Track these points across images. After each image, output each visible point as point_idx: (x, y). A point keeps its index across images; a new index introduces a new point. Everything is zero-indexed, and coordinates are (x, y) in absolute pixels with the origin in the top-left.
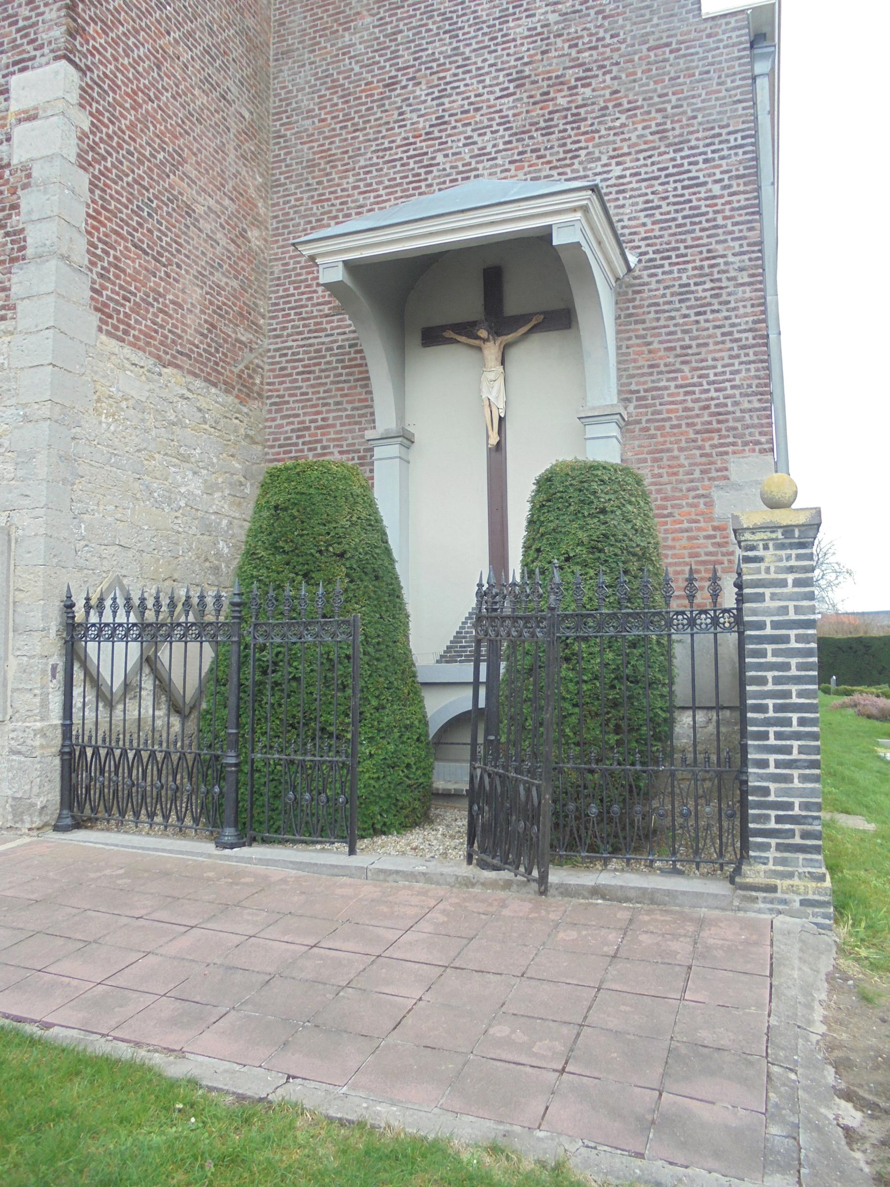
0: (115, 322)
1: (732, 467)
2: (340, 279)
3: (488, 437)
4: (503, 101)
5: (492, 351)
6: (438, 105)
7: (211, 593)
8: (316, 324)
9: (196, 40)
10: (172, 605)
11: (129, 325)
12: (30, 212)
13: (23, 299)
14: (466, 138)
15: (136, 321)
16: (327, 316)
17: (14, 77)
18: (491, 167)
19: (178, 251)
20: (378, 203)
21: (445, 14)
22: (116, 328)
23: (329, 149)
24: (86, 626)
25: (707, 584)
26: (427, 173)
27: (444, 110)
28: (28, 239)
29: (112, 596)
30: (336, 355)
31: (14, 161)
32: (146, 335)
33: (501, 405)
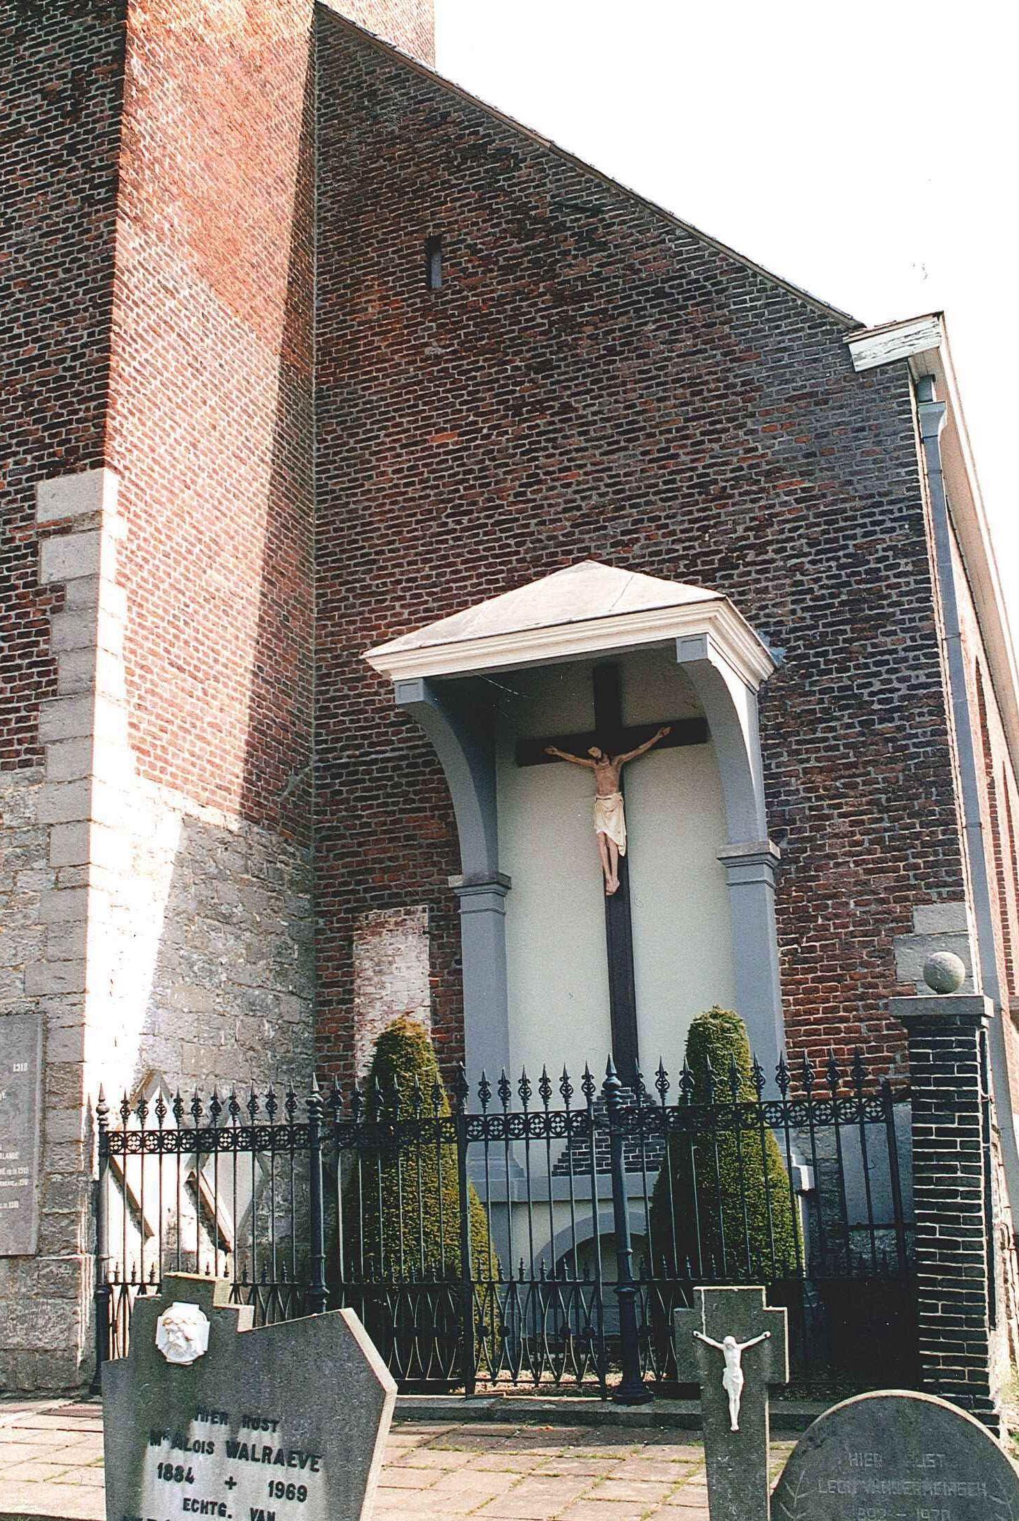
0: (152, 759)
1: (917, 918)
2: (421, 699)
3: (605, 881)
4: (612, 457)
5: (609, 774)
6: (529, 461)
7: (262, 1091)
8: (379, 735)
9: (232, 402)
10: (216, 1108)
11: (166, 762)
12: (63, 641)
13: (54, 742)
14: (566, 502)
15: (174, 755)
16: (392, 724)
17: (41, 482)
18: (598, 538)
19: (216, 661)
20: (455, 581)
21: (535, 349)
22: (152, 766)
23: (391, 511)
24: (124, 1138)
25: (849, 1069)
26: (518, 544)
27: (537, 467)
28: (60, 671)
29: (156, 1096)
30: (406, 775)
31: (43, 580)
32: (183, 770)
33: (621, 841)
